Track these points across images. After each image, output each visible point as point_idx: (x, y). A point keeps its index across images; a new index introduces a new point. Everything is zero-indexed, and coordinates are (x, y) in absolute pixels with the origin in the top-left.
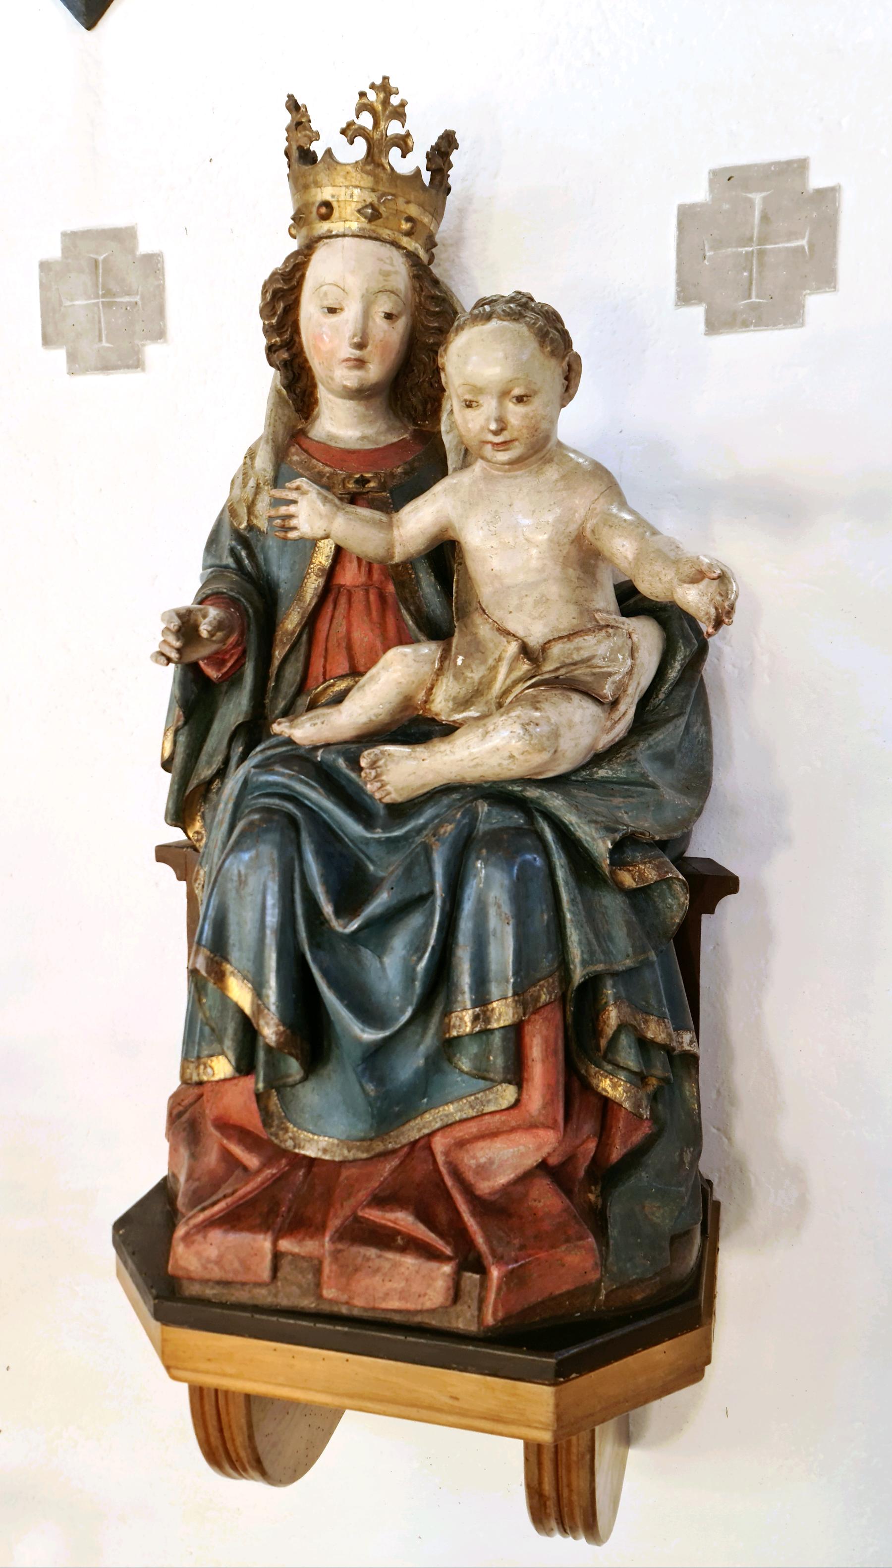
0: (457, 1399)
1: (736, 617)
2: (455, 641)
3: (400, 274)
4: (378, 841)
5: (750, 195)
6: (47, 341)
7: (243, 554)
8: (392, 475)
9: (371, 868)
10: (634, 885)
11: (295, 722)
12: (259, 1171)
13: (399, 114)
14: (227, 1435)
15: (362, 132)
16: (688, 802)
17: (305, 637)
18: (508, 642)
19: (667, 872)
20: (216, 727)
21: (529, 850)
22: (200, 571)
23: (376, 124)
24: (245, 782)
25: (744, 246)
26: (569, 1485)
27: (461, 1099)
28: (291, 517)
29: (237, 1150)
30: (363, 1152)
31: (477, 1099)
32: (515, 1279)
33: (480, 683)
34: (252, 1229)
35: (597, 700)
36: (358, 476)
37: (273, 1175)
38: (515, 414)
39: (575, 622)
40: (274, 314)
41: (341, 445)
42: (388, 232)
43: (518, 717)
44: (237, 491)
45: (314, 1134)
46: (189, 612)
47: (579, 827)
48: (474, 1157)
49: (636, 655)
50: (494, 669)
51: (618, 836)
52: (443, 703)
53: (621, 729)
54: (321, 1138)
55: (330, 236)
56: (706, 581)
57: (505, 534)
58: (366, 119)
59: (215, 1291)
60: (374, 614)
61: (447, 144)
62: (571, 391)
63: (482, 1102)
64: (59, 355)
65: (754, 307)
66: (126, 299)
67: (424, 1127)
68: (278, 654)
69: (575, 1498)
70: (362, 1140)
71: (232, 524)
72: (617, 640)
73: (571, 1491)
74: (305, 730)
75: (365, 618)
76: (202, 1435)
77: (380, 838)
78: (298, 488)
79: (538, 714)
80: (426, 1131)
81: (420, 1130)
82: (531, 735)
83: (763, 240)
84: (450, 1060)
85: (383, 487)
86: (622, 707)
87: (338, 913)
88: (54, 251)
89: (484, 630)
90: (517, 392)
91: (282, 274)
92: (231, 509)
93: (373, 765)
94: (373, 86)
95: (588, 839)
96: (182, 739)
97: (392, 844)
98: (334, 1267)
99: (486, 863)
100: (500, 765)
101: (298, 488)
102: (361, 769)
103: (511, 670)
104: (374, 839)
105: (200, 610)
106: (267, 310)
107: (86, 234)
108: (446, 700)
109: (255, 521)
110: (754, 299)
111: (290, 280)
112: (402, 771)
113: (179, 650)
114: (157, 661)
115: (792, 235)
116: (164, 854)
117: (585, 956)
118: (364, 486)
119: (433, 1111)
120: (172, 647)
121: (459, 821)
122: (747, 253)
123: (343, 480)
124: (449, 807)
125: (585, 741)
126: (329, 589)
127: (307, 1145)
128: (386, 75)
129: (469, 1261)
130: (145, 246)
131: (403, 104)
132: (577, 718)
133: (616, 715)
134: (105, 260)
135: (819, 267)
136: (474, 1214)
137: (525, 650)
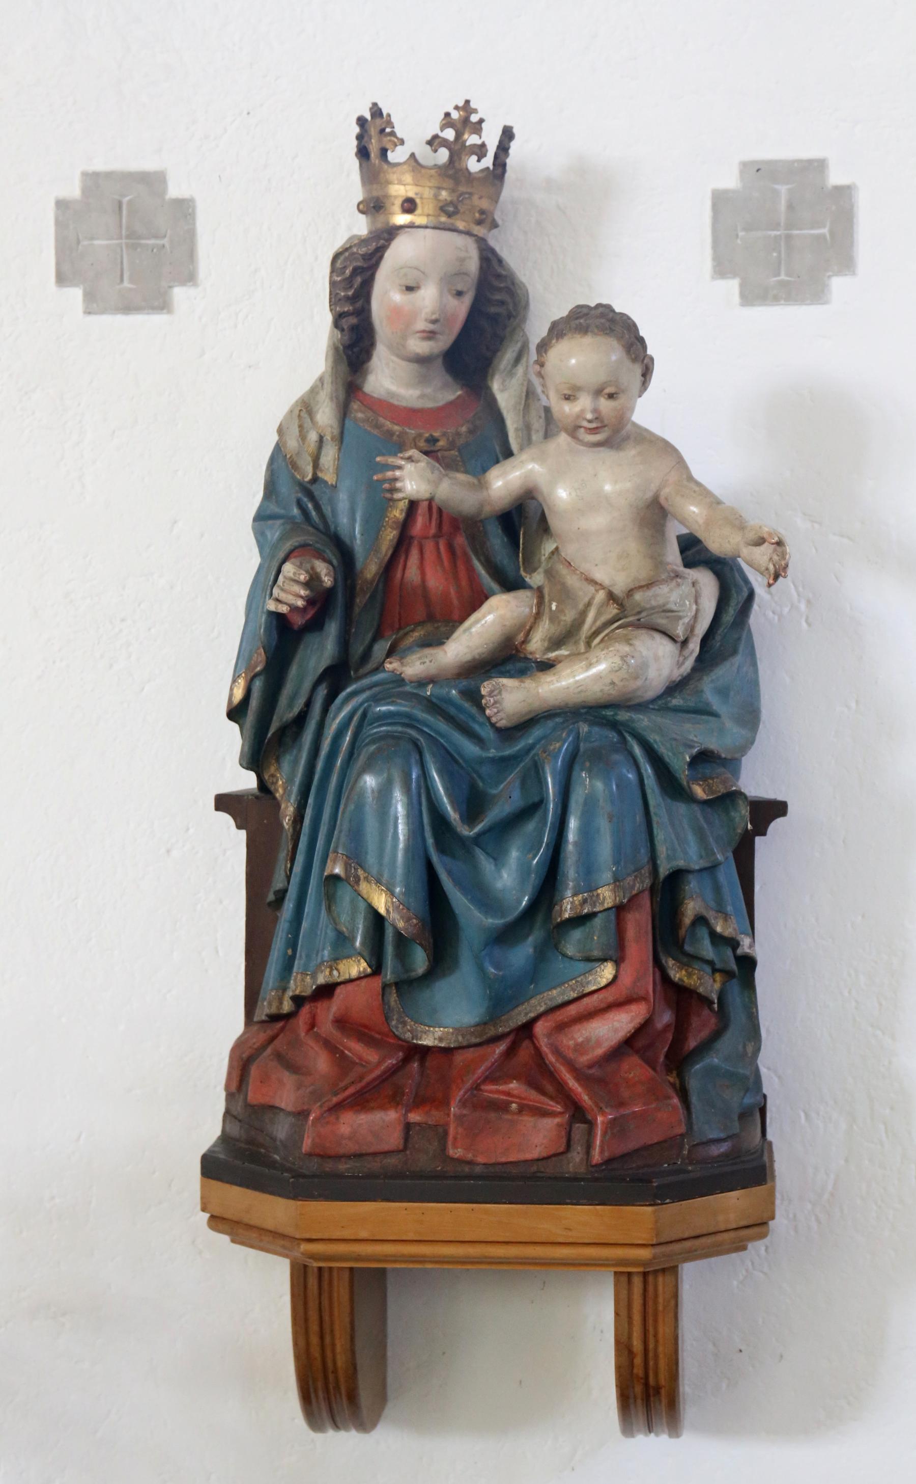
0: (570, 1230)
1: (790, 571)
3: (473, 265)
4: (493, 760)
5: (777, 187)
6: (61, 279)
7: (310, 506)
8: (458, 434)
9: (481, 784)
10: (705, 797)
11: (405, 661)
12: (379, 1063)
14: (328, 1340)
15: (445, 143)
16: (744, 732)
17: (381, 586)
18: (597, 591)
23: (459, 135)
25: (773, 230)
26: (656, 1335)
27: (563, 984)
28: (396, 479)
30: (476, 1037)
31: (577, 982)
32: (617, 1127)
33: (572, 626)
34: (382, 1107)
35: (673, 639)
36: (427, 435)
37: (393, 1065)
38: (605, 405)
39: (652, 573)
40: (351, 287)
41: (404, 404)
45: (429, 1026)
47: (663, 744)
48: (573, 1038)
50: (583, 614)
52: (539, 643)
53: (689, 664)
54: (437, 1029)
56: (766, 544)
57: (583, 495)
59: (348, 1166)
61: (508, 134)
63: (581, 984)
64: (76, 294)
65: (783, 284)
66: (152, 242)
67: (530, 1011)
70: (477, 1025)
72: (686, 588)
73: (657, 1341)
74: (415, 666)
75: (438, 568)
76: (302, 1343)
81: (526, 1014)
82: (628, 666)
83: (790, 226)
84: (556, 947)
85: (452, 445)
88: (73, 191)
90: (609, 390)
91: (363, 255)
93: (490, 694)
94: (456, 108)
95: (670, 754)
96: (258, 684)
97: (505, 763)
98: (460, 1130)
99: (589, 771)
100: (602, 691)
103: (599, 614)
107: (109, 175)
108: (543, 640)
109: (320, 475)
110: (783, 277)
111: (370, 259)
112: (510, 697)
115: (815, 224)
116: (223, 803)
117: (669, 852)
119: (538, 997)
122: (776, 237)
123: (414, 439)
124: (554, 729)
125: (665, 672)
126: (403, 543)
128: (468, 98)
129: (578, 1113)
130: (174, 191)
131: (481, 121)
132: (660, 653)
133: (686, 652)
134: (130, 202)
135: (838, 250)
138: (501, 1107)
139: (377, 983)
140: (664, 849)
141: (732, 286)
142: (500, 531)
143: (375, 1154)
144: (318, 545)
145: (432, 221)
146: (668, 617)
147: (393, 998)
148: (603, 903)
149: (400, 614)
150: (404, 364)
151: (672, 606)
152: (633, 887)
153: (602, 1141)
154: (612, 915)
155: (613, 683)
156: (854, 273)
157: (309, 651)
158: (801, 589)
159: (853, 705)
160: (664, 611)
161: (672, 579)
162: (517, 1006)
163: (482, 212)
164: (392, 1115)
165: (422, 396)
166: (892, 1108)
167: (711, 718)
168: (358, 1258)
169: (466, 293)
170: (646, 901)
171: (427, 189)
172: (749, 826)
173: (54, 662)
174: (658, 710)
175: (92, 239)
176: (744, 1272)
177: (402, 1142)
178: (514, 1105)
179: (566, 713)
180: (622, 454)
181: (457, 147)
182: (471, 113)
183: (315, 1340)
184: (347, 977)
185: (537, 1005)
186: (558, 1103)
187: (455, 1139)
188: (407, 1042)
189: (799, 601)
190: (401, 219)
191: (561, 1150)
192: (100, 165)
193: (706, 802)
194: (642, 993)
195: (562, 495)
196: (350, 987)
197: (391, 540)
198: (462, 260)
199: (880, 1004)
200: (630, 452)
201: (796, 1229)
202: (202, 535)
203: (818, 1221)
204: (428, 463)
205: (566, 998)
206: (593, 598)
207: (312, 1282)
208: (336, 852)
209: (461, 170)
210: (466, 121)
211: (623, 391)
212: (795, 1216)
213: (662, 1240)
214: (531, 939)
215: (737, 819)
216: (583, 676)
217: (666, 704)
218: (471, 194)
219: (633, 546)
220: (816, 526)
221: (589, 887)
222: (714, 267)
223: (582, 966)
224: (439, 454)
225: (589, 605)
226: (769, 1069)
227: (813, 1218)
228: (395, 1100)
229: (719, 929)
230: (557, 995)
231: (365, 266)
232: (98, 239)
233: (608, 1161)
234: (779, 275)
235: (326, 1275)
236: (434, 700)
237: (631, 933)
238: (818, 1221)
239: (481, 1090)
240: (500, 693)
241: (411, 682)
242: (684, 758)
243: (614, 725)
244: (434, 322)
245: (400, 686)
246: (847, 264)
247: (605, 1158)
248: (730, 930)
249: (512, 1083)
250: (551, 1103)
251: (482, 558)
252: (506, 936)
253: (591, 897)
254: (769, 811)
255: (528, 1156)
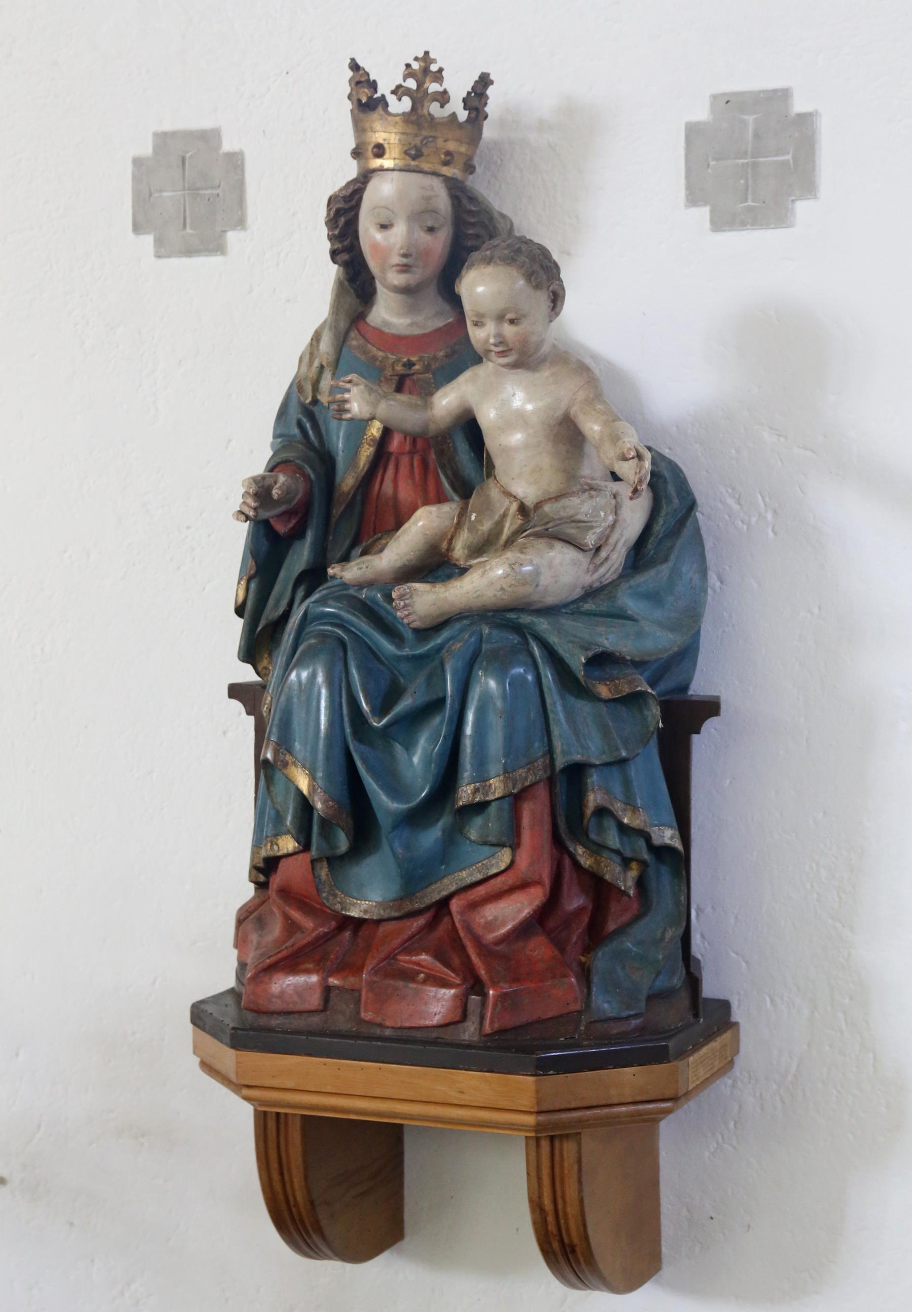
0: (462, 1092)
2: (471, 501)
3: (443, 201)
4: (408, 658)
5: (745, 117)
6: (137, 228)
7: (308, 425)
8: (435, 358)
9: (402, 681)
13: (438, 76)
14: (286, 1177)
15: (408, 92)
17: (359, 498)
19: (637, 686)
20: (282, 574)
21: (520, 664)
22: (271, 439)
23: (420, 85)
24: (305, 614)
26: (563, 1198)
27: (471, 866)
28: (346, 401)
29: (296, 915)
30: (396, 912)
33: (489, 535)
34: (308, 972)
35: (580, 547)
36: (405, 360)
38: (509, 331)
40: (337, 227)
41: (394, 331)
42: (430, 165)
43: (507, 559)
44: (304, 368)
45: (357, 899)
46: (263, 478)
48: (484, 917)
49: (619, 512)
50: (500, 524)
51: (590, 654)
55: (382, 169)
58: (411, 84)
60: (417, 476)
61: (484, 81)
62: (557, 310)
64: (148, 240)
65: (750, 209)
67: (443, 890)
68: (337, 511)
69: (569, 1210)
70: (394, 900)
71: (299, 400)
72: (600, 500)
73: (565, 1202)
77: (408, 655)
78: (350, 382)
79: (523, 556)
80: (445, 893)
81: (439, 892)
85: (427, 368)
86: (603, 554)
87: (373, 711)
88: (146, 149)
89: (494, 493)
92: (297, 386)
93: (401, 597)
94: (416, 59)
96: (253, 585)
98: (370, 995)
100: (495, 596)
101: (350, 382)
102: (393, 600)
104: (403, 656)
105: (271, 477)
106: (331, 222)
107: (174, 134)
108: (463, 548)
109: (319, 397)
110: (750, 203)
112: (425, 600)
113: (255, 509)
114: (238, 519)
115: (780, 151)
116: (236, 691)
117: (565, 747)
118: (410, 369)
120: (250, 507)
121: (467, 641)
122: (743, 164)
127: (352, 908)
129: (476, 986)
130: (228, 146)
131: (441, 70)
133: (598, 561)
134: (191, 157)
136: (479, 955)
137: (523, 509)
138: (408, 976)
139: (305, 858)
140: (560, 744)
141: (703, 213)
142: (467, 447)
143: (300, 1012)
144: (298, 461)
145: (400, 163)
146: (578, 527)
147: (324, 872)
148: (494, 793)
149: (375, 524)
150: (392, 295)
151: (581, 517)
152: (526, 778)
153: (492, 1013)
154: (506, 805)
155: (502, 589)
156: (815, 197)
157: (295, 557)
158: (767, 499)
159: (816, 610)
160: (573, 521)
161: (584, 491)
162: (431, 884)
163: (448, 153)
164: (314, 978)
165: (411, 325)
166: (851, 998)
167: (628, 622)
168: (290, 1105)
169: (439, 228)
170: (542, 792)
171: (393, 135)
172: (661, 724)
173: (134, 565)
174: (572, 614)
175: (161, 191)
176: (715, 1145)
177: (321, 1003)
178: (422, 975)
179: (472, 616)
180: (537, 375)
181: (420, 95)
182: (431, 63)
183: (276, 1176)
184: (285, 851)
185: (448, 885)
186: (458, 975)
187: (366, 1003)
188: (338, 912)
189: (766, 511)
190: (377, 163)
191: (457, 1019)
192: (168, 126)
193: (606, 701)
194: (536, 877)
195: (488, 417)
196: (291, 860)
197: (368, 456)
198: (427, 199)
199: (840, 898)
200: (545, 373)
201: (762, 1109)
202: (252, 452)
203: (783, 1101)
204: (366, 386)
205: (474, 879)
206: (508, 509)
207: (271, 1124)
208: (269, 739)
209: (424, 116)
210: (426, 71)
211: (524, 316)
212: (761, 1095)
213: (544, 1109)
214: (440, 824)
215: (649, 718)
216: (485, 581)
217: (578, 608)
218: (435, 138)
219: (546, 461)
220: (782, 439)
221: (482, 778)
222: (687, 196)
223: (487, 850)
224: (415, 377)
225: (504, 515)
226: (737, 954)
227: (778, 1098)
228: (321, 965)
229: (626, 821)
230: (467, 876)
231: (346, 207)
232: (165, 191)
233: (502, 1031)
234: (746, 200)
235: (282, 1120)
236: (369, 603)
237: (526, 821)
238: (783, 1101)
239: (397, 960)
240: (411, 597)
241: (354, 586)
242: (580, 659)
243: (518, 629)
244: (405, 256)
245: (346, 589)
246: (809, 188)
247: (495, 1029)
248: (638, 822)
249: (421, 954)
250: (453, 975)
251: (449, 472)
252: (417, 818)
253: (484, 787)
254: (711, 708)
255: (428, 1023)
